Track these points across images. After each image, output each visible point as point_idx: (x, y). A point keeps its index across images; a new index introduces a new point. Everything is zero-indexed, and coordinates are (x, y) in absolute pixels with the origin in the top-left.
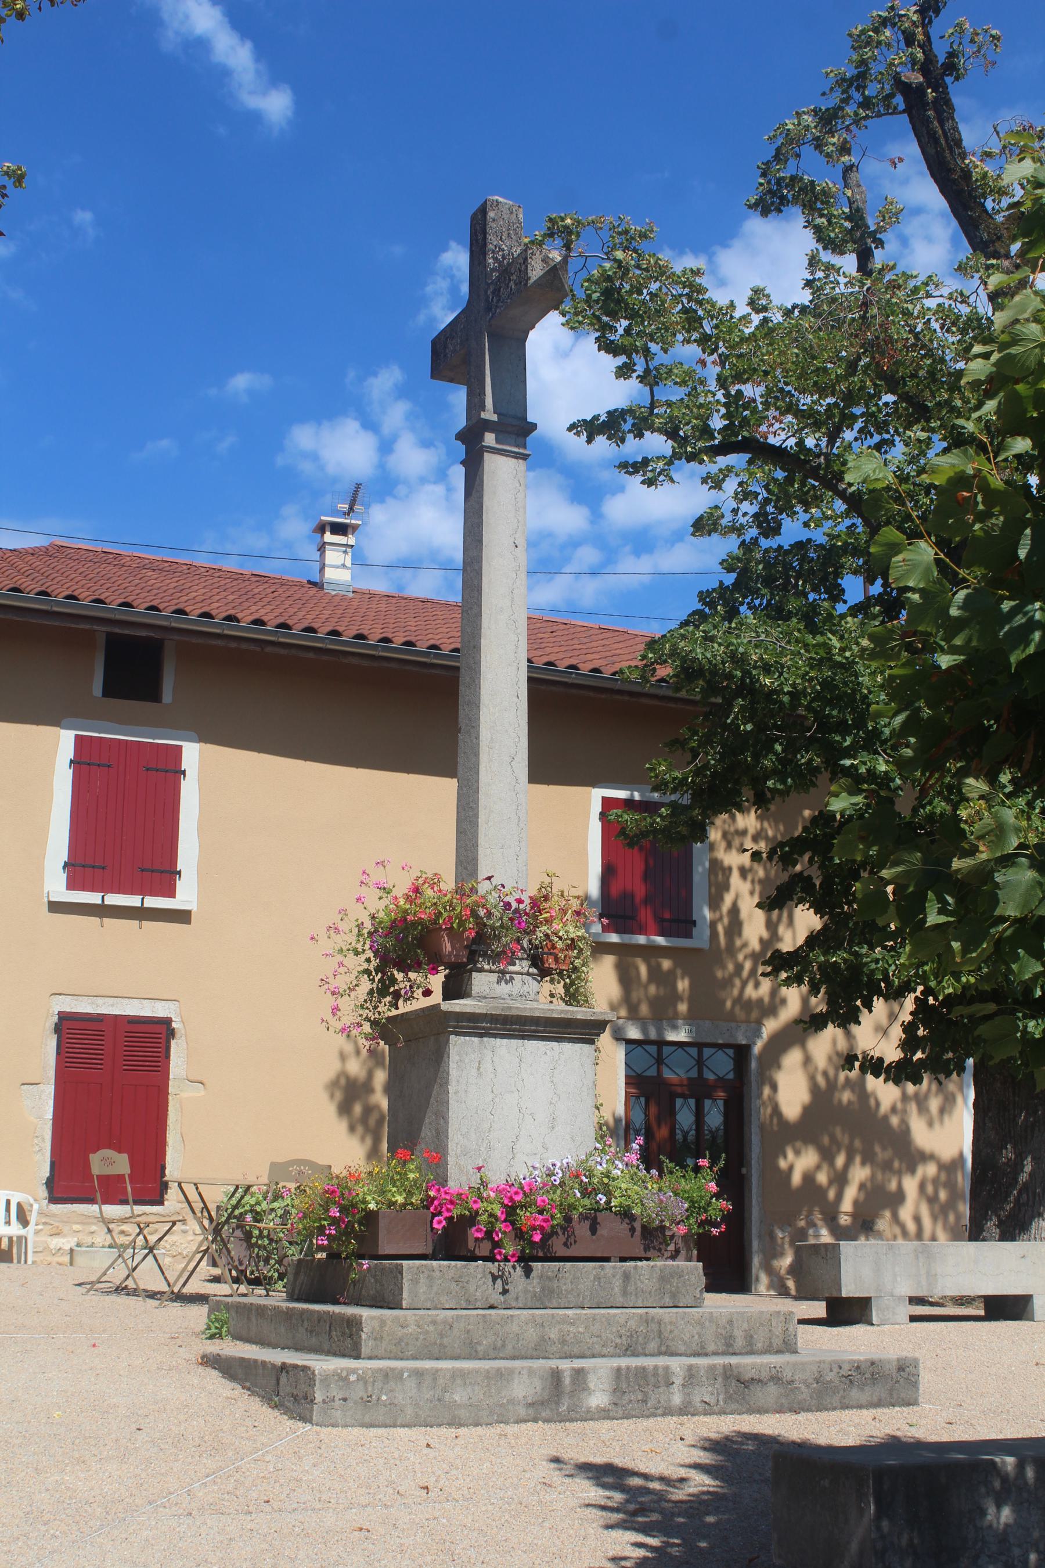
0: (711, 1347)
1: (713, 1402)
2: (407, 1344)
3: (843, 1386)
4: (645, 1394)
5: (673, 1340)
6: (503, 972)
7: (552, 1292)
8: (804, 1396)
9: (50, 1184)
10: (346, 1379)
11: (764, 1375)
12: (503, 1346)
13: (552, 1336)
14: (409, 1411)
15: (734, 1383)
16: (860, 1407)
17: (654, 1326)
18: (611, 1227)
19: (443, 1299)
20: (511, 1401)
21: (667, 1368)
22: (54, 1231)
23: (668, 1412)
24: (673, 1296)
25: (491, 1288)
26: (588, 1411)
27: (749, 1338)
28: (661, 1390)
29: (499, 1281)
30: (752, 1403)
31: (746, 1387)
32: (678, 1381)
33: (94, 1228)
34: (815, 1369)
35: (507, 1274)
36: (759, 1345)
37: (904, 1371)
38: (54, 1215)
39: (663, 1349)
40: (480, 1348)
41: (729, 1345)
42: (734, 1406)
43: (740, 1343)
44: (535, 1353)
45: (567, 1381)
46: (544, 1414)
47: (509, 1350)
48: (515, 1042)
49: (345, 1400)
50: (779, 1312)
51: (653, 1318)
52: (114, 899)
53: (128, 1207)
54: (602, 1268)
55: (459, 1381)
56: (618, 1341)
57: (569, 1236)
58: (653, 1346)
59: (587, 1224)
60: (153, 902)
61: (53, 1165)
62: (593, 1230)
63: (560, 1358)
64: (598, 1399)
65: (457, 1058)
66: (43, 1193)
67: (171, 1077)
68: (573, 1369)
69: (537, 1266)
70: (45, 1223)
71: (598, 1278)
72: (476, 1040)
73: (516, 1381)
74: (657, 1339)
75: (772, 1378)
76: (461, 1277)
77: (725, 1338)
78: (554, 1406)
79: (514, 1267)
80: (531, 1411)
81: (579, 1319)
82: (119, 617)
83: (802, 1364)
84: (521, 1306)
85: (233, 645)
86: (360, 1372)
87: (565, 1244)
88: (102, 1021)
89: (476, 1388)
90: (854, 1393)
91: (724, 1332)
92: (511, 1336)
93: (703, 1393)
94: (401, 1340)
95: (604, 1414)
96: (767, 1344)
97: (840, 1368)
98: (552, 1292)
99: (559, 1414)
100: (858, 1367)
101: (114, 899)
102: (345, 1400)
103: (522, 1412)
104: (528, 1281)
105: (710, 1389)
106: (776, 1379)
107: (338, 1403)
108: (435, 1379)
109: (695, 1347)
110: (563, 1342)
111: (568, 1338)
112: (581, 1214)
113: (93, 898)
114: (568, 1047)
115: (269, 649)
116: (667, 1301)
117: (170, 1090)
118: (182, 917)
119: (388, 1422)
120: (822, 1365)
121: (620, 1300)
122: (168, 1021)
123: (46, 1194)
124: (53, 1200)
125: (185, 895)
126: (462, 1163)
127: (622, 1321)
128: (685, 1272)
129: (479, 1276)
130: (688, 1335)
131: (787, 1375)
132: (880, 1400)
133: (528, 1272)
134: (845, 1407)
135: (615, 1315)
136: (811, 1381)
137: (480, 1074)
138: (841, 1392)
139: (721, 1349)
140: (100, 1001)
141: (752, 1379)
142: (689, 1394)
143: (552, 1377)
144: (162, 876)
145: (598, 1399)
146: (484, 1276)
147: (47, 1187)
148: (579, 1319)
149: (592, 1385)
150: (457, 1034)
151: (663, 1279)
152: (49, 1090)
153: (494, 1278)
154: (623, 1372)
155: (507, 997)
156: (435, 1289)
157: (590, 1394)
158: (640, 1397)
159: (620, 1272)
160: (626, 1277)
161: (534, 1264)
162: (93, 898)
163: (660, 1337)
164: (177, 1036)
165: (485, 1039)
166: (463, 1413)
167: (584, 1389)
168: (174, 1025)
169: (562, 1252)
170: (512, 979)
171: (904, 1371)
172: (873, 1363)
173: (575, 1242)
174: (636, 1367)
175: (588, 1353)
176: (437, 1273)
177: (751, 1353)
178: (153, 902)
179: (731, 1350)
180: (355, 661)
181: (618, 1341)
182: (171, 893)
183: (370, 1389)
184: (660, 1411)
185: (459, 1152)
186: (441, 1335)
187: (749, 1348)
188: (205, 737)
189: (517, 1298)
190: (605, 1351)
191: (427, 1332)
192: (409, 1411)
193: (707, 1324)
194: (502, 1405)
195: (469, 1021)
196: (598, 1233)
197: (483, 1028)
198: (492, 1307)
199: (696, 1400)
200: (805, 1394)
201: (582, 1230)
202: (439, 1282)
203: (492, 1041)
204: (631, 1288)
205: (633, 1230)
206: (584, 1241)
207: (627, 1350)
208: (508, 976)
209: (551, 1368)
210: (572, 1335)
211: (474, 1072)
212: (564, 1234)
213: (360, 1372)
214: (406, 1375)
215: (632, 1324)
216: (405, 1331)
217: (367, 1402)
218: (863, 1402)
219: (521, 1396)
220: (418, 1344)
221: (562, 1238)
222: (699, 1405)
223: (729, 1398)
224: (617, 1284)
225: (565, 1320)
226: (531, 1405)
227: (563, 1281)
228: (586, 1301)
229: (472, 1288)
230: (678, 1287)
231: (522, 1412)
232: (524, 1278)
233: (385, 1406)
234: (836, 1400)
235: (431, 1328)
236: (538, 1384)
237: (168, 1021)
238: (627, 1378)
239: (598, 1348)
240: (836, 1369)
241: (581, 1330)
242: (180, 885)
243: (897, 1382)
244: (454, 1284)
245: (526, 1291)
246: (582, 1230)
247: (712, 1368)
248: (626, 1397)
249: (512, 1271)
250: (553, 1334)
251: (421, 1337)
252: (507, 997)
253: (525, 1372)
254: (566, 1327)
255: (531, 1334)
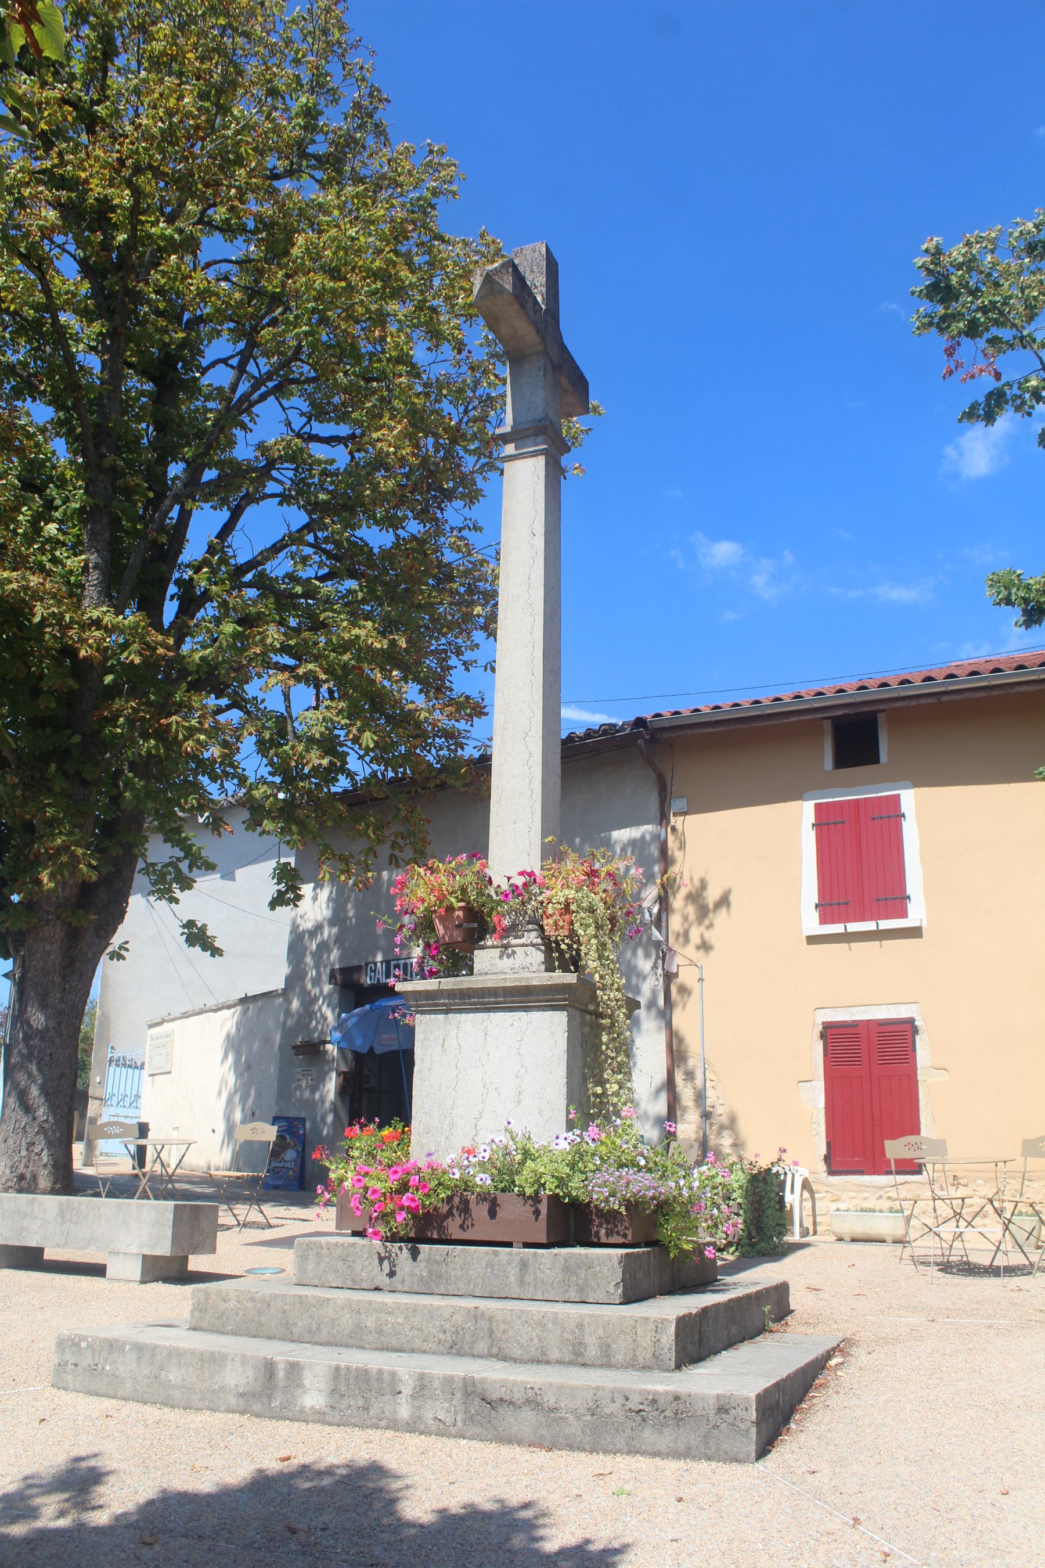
0: (555, 1354)
1: (449, 1421)
2: (228, 1318)
3: (630, 1423)
4: (367, 1401)
5: (507, 1341)
6: (506, 947)
7: (440, 1277)
8: (573, 1430)
9: (827, 1159)
10: (78, 1345)
11: (518, 1396)
12: (319, 1330)
13: (369, 1324)
14: (129, 1384)
15: (477, 1401)
16: (655, 1454)
17: (484, 1324)
18: (512, 1209)
19: (330, 1277)
20: (223, 1388)
21: (393, 1374)
22: (834, 1198)
23: (394, 1425)
24: (581, 1289)
25: (377, 1269)
26: (302, 1411)
27: (606, 1349)
28: (386, 1398)
29: (386, 1263)
30: (500, 1429)
31: (493, 1408)
32: (407, 1390)
33: (866, 1195)
34: (589, 1397)
35: (394, 1255)
36: (619, 1357)
37: (727, 1412)
38: (832, 1185)
39: (495, 1350)
40: (295, 1330)
41: (578, 1353)
42: (477, 1430)
43: (592, 1352)
44: (350, 1341)
45: (281, 1374)
46: (254, 1407)
47: (324, 1335)
48: (480, 1016)
49: (76, 1365)
50: (647, 1319)
51: (483, 1314)
52: (854, 927)
53: (891, 1177)
54: (496, 1254)
55: (174, 1361)
56: (442, 1336)
57: (465, 1219)
58: (482, 1346)
59: (486, 1206)
60: (885, 924)
61: (828, 1144)
62: (492, 1214)
63: (376, 1349)
64: (314, 1398)
65: (422, 1036)
66: (822, 1167)
67: (919, 1066)
68: (288, 1362)
69: (424, 1248)
70: (827, 1192)
71: (490, 1265)
72: (441, 1017)
73: (229, 1368)
74: (487, 1339)
75: (528, 1401)
76: (347, 1256)
77: (574, 1346)
78: (265, 1400)
79: (401, 1248)
80: (241, 1402)
81: (398, 1308)
82: (859, 699)
83: (573, 1388)
84: (407, 1290)
85: (913, 703)
86: (90, 1340)
87: (462, 1227)
88: (857, 1026)
89: (190, 1369)
90: (648, 1436)
91: (571, 1338)
92: (326, 1320)
93: (437, 1410)
94: (223, 1314)
95: (320, 1418)
96: (629, 1357)
97: (627, 1399)
98: (440, 1277)
99: (271, 1409)
100: (654, 1401)
101: (854, 927)
102: (76, 1365)
103: (233, 1401)
104: (415, 1264)
105: (446, 1405)
106: (533, 1402)
107: (70, 1367)
108: (153, 1355)
109: (533, 1353)
110: (380, 1332)
111: (385, 1328)
112: (479, 1195)
113: (837, 928)
114: (536, 1016)
115: (945, 698)
116: (573, 1295)
117: (919, 1078)
118: (915, 932)
119: (110, 1392)
120: (600, 1393)
121: (516, 1291)
122: (911, 1021)
123: (825, 1168)
124: (831, 1172)
125: (916, 914)
126: (424, 1141)
127: (446, 1314)
128: (596, 1262)
129: (366, 1256)
130: (526, 1338)
131: (549, 1400)
132: (689, 1449)
133: (415, 1254)
134: (632, 1451)
135: (439, 1308)
136: (581, 1411)
137: (444, 1051)
138: (628, 1431)
139: (568, 1357)
140: (854, 1010)
141: (501, 1400)
142: (419, 1408)
143: (266, 1368)
144: (896, 901)
145: (314, 1398)
146: (370, 1257)
147: (826, 1162)
148: (398, 1308)
149: (307, 1383)
150: (422, 1013)
151: (567, 1269)
152: (820, 1085)
153: (381, 1260)
154: (342, 1372)
155: (508, 970)
156: (323, 1266)
157: (305, 1392)
158: (360, 1404)
159: (517, 1259)
160: (524, 1265)
161: (422, 1247)
162: (837, 928)
163: (491, 1337)
164: (920, 1032)
165: (450, 1015)
166: (176, 1394)
167: (298, 1386)
168: (917, 1023)
169: (457, 1234)
170: (514, 952)
171: (727, 1412)
172: (677, 1398)
173: (473, 1225)
174: (357, 1368)
175: (406, 1347)
176: (325, 1251)
177: (609, 1365)
178: (885, 924)
179: (580, 1360)
180: (1022, 689)
181: (442, 1336)
182: (904, 914)
183: (97, 1357)
184: (383, 1423)
185: (421, 1130)
186: (260, 1313)
187: (605, 1360)
188: (919, 781)
189: (403, 1281)
190: (426, 1346)
191: (246, 1309)
192: (129, 1384)
193: (550, 1326)
194: (213, 1391)
195: (427, 999)
196: (499, 1215)
197: (445, 1005)
198: (377, 1289)
199: (429, 1415)
200: (574, 1427)
201: (479, 1211)
202: (327, 1260)
203: (457, 1017)
204: (529, 1278)
205: (537, 1213)
206: (482, 1227)
207: (451, 1347)
208: (510, 951)
209: (265, 1358)
210: (390, 1325)
211: (439, 1049)
212: (460, 1215)
213: (90, 1340)
214: (128, 1347)
215: (458, 1319)
216: (226, 1305)
217: (93, 1369)
218: (663, 1448)
219: (232, 1384)
220: (238, 1319)
221: (458, 1220)
222: (431, 1422)
223: (470, 1419)
224: (513, 1272)
225: (383, 1308)
226: (242, 1395)
227: (451, 1266)
228: (477, 1289)
229: (358, 1268)
230: (586, 1280)
231: (233, 1401)
232: (410, 1261)
233: (108, 1376)
234: (620, 1441)
235: (250, 1305)
236: (250, 1373)
237: (911, 1021)
238: (347, 1379)
239: (418, 1343)
240: (620, 1401)
241: (400, 1320)
242: (911, 907)
243: (715, 1427)
244: (341, 1263)
245: (412, 1275)
246: (479, 1211)
247: (449, 1380)
248: (345, 1402)
249: (398, 1252)
250: (370, 1322)
251: (241, 1313)
252: (508, 970)
253: (238, 1359)
254: (383, 1317)
255: (347, 1320)
